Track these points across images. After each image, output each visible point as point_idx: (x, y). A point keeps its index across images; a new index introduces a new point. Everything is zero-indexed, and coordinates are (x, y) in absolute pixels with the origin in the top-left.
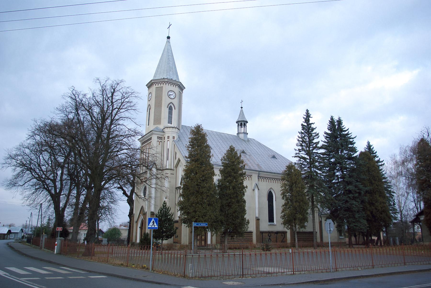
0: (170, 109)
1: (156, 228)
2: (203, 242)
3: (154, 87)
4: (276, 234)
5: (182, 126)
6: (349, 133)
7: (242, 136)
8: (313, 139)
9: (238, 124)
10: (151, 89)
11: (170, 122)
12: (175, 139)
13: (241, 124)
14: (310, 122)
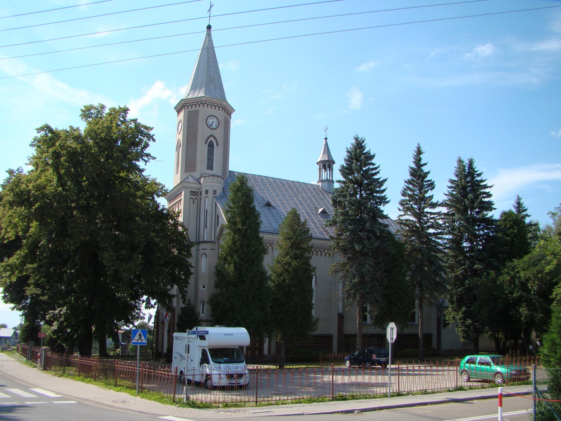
1: (145, 343)
2: (257, 352)
5: (230, 172)
6: (484, 179)
8: (427, 192)
9: (320, 166)
11: (210, 166)
12: (218, 194)
14: (422, 163)
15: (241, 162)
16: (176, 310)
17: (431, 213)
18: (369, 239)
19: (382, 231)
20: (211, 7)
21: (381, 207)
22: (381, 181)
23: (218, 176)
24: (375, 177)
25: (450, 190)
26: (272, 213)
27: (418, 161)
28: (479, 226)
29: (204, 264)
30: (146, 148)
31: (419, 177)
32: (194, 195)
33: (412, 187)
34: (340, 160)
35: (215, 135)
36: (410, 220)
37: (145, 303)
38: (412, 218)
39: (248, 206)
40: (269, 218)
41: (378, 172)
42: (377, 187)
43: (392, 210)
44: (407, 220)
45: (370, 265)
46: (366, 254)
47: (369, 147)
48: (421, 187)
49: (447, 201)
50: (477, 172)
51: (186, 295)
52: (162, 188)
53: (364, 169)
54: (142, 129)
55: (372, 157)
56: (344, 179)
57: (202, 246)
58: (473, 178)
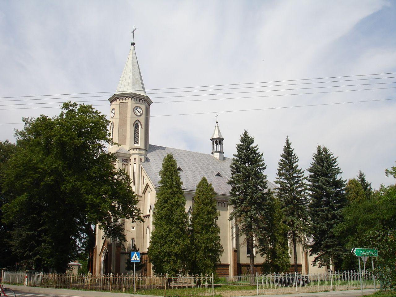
0: (136, 126)
1: (139, 261)
3: (118, 102)
9: (213, 142)
13: (216, 142)
20: (133, 31)
31: (288, 154)
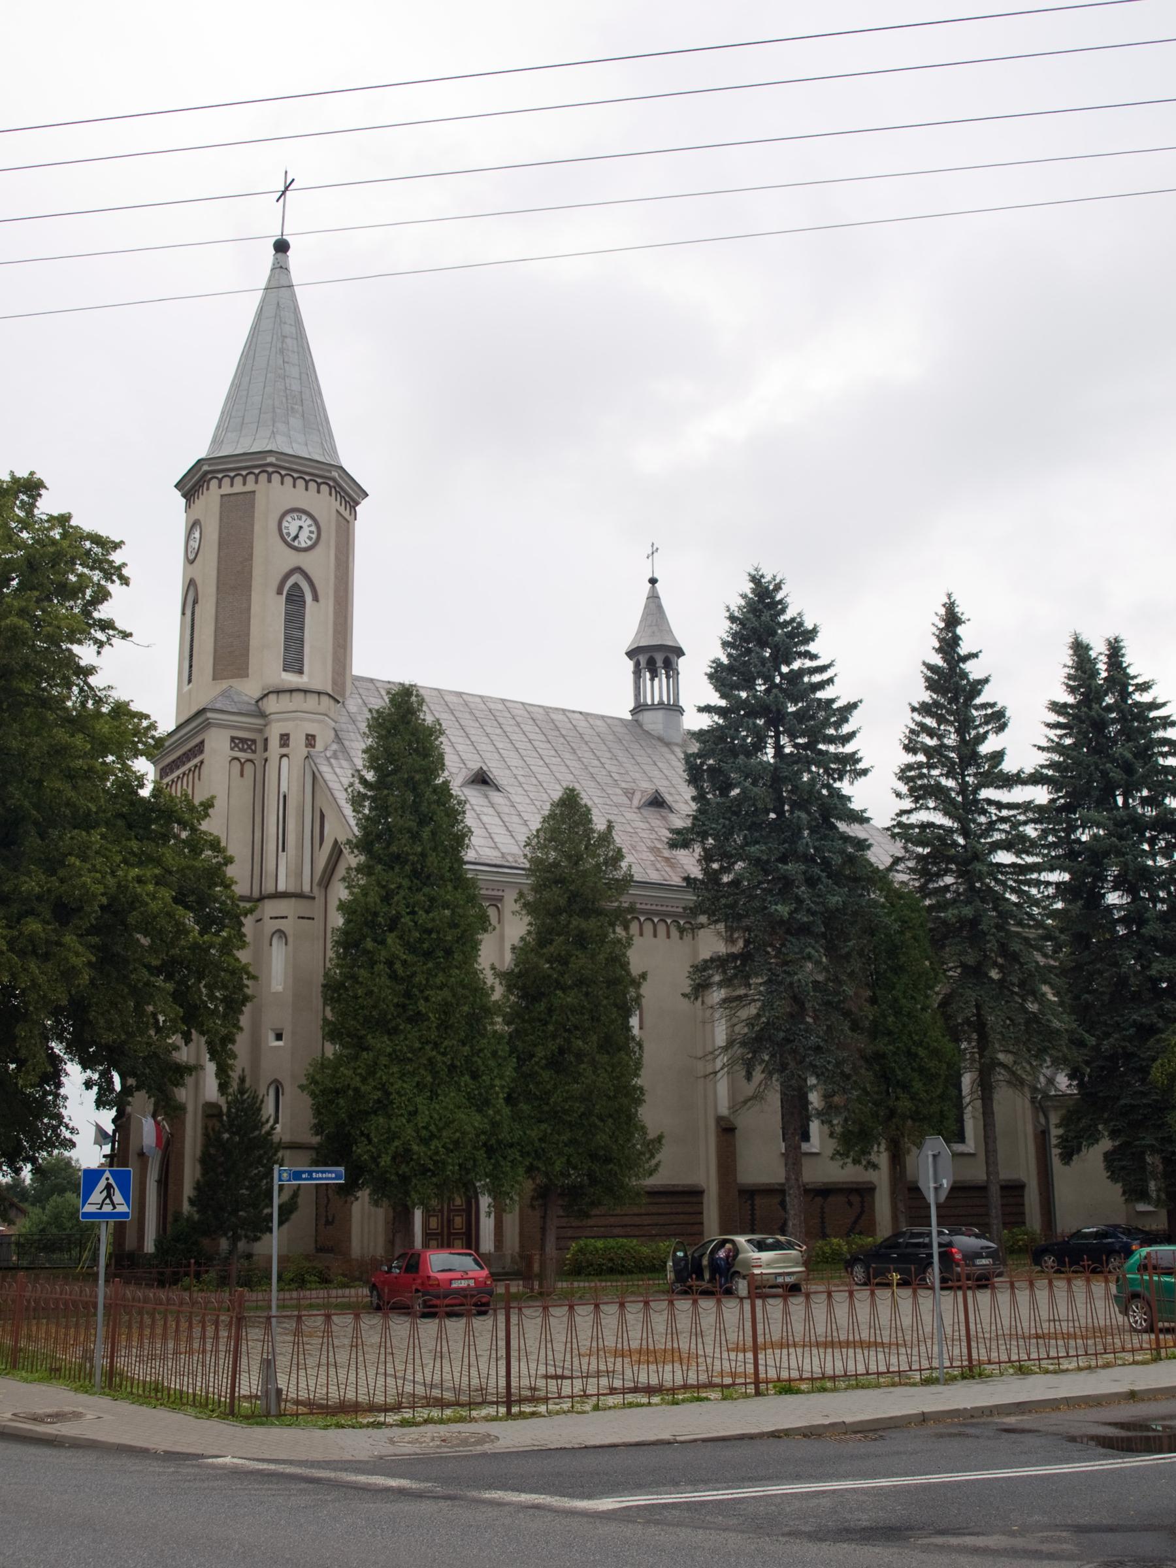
0: (295, 600)
1: (125, 1215)
3: (212, 496)
4: (819, 1200)
6: (1159, 701)
7: (654, 721)
8: (982, 738)
9: (637, 664)
10: (200, 502)
11: (294, 663)
14: (963, 650)
15: (390, 645)
16: (190, 1108)
17: (1000, 805)
18: (811, 882)
19: (851, 860)
21: (845, 787)
22: (840, 709)
23: (319, 693)
24: (820, 695)
25: (1053, 734)
26: (492, 805)
27: (949, 644)
28: (1152, 841)
29: (285, 964)
30: (101, 602)
31: (953, 689)
32: (242, 750)
33: (935, 725)
34: (704, 641)
35: (304, 567)
36: (931, 825)
37: (95, 1089)
38: (939, 819)
39: (428, 782)
40: (485, 819)
41: (830, 681)
42: (829, 725)
43: (877, 796)
44: (924, 826)
45: (818, 963)
46: (804, 930)
47: (800, 603)
48: (964, 724)
49: (1048, 767)
50: (1135, 677)
51: (231, 1067)
52: (149, 728)
53: (785, 669)
54: (88, 544)
55: (810, 635)
56: (723, 703)
57: (270, 908)
58: (1124, 695)
